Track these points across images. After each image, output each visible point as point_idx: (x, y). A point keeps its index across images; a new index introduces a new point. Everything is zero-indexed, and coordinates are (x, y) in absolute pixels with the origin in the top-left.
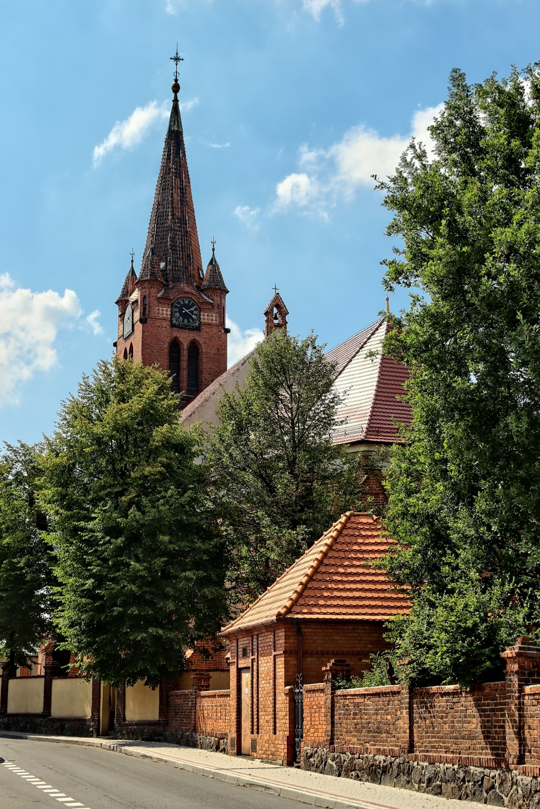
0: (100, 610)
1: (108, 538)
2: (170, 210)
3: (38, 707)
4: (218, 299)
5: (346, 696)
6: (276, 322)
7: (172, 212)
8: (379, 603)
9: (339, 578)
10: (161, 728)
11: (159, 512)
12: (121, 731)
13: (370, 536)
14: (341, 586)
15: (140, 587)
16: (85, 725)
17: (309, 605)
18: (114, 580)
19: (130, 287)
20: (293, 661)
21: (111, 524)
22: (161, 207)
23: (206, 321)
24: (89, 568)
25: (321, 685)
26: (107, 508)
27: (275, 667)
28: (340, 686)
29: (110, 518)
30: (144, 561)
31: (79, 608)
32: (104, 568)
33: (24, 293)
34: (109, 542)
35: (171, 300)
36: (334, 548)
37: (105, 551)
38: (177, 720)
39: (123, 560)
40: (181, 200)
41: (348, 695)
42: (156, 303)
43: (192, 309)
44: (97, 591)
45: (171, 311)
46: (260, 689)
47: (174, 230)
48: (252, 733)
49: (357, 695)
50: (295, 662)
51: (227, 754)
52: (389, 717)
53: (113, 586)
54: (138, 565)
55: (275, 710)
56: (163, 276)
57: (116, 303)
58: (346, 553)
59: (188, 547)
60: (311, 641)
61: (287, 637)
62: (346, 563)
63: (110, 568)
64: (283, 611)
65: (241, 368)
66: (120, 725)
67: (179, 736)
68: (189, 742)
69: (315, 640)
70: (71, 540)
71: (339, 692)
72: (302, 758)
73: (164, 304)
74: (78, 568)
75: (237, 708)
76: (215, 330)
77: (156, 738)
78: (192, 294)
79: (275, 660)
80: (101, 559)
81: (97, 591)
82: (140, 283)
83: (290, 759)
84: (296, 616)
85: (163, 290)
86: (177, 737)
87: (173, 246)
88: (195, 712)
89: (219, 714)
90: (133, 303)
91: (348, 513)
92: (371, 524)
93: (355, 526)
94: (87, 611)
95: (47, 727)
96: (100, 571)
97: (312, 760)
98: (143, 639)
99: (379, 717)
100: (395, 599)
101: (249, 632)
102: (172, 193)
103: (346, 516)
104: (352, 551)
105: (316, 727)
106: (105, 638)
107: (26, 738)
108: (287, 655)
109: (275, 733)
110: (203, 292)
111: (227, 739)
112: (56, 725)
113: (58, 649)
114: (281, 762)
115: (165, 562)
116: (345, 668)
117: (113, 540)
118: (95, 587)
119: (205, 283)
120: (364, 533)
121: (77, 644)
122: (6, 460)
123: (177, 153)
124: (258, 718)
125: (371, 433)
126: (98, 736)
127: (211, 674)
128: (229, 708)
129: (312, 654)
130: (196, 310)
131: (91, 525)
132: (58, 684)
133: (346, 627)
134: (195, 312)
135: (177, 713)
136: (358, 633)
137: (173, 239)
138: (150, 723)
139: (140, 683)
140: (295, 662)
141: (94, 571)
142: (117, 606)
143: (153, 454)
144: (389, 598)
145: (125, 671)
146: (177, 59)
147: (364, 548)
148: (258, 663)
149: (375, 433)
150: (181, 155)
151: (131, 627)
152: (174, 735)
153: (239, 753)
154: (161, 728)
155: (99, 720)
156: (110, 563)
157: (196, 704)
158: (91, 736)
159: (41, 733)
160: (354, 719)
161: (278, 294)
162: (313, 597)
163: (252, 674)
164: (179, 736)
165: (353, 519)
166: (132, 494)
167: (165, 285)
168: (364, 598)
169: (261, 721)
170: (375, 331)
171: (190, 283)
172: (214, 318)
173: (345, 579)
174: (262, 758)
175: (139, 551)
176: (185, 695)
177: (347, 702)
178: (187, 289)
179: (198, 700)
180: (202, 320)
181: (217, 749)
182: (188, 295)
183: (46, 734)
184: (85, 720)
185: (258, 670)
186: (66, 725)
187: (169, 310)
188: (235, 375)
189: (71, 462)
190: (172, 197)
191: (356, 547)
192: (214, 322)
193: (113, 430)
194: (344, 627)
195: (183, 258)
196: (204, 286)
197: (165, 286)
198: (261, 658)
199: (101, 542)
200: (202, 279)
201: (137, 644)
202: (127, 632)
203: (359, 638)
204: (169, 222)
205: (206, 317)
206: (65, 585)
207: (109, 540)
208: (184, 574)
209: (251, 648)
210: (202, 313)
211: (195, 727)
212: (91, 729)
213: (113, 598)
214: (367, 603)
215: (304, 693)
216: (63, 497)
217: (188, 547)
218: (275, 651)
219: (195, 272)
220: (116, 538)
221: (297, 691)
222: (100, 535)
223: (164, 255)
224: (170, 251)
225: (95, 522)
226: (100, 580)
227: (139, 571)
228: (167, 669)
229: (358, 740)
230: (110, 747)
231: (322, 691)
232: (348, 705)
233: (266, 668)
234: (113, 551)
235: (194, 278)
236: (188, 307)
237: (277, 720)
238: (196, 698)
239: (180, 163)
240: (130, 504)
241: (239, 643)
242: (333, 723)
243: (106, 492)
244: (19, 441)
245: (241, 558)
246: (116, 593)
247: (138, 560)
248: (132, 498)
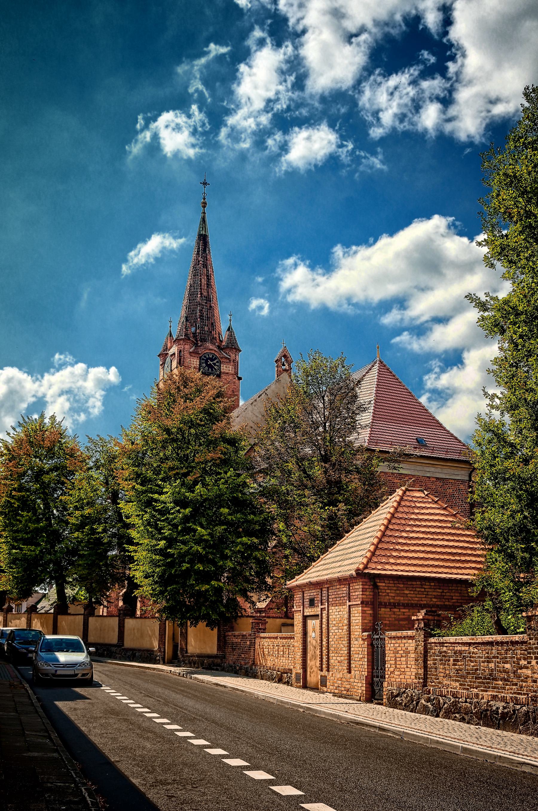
0: (170, 565)
3: (114, 639)
5: (443, 643)
6: (284, 367)
8: (441, 564)
10: (219, 661)
12: (184, 661)
14: (406, 548)
15: (204, 549)
18: (184, 543)
25: (410, 633)
27: (349, 616)
30: (207, 528)
33: (80, 367)
34: (178, 511)
36: (396, 516)
37: (175, 518)
41: (446, 643)
42: (189, 356)
43: (215, 362)
45: (200, 362)
46: (330, 634)
50: (371, 612)
51: (291, 685)
52: (507, 666)
54: (203, 530)
56: (194, 337)
62: (408, 529)
66: (183, 656)
67: (238, 668)
68: (250, 672)
70: (146, 509)
71: (432, 640)
75: (303, 649)
80: (172, 525)
83: (368, 696)
84: (372, 572)
87: (201, 316)
90: (171, 355)
93: (411, 499)
94: (159, 566)
96: (170, 534)
97: (398, 699)
98: (207, 591)
99: (492, 665)
100: (453, 560)
101: (318, 585)
103: (402, 490)
104: (411, 519)
105: (403, 670)
106: (175, 588)
107: (106, 662)
109: (350, 672)
111: (291, 674)
115: (225, 529)
116: (436, 618)
117: (182, 510)
118: (166, 548)
119: (224, 344)
122: (88, 450)
123: (204, 250)
126: (164, 663)
127: (267, 620)
129: (385, 606)
130: (217, 362)
131: (163, 498)
132: (129, 623)
133: (414, 583)
135: (234, 650)
137: (201, 311)
138: (209, 656)
139: (202, 625)
140: (371, 612)
142: (185, 562)
148: (328, 611)
152: (231, 666)
153: (305, 686)
155: (164, 652)
156: (180, 528)
158: (159, 664)
159: (115, 659)
163: (321, 621)
164: (238, 668)
165: (408, 493)
166: (197, 474)
167: (195, 344)
169: (332, 661)
174: (334, 693)
175: (203, 520)
176: (243, 636)
178: (211, 347)
179: (258, 641)
183: (120, 659)
184: (153, 651)
185: (328, 617)
191: (413, 516)
194: (413, 583)
197: (196, 345)
200: (221, 341)
203: (425, 593)
206: (141, 544)
208: (240, 539)
209: (319, 599)
213: (182, 556)
214: (431, 563)
216: (138, 475)
218: (349, 601)
219: (217, 336)
220: (185, 509)
221: (376, 637)
226: (171, 542)
227: (203, 535)
229: (461, 685)
230: (179, 674)
231: (411, 638)
233: (338, 616)
236: (212, 360)
241: (305, 595)
242: (425, 667)
243: (174, 472)
244: (98, 436)
245: (280, 531)
247: (202, 527)
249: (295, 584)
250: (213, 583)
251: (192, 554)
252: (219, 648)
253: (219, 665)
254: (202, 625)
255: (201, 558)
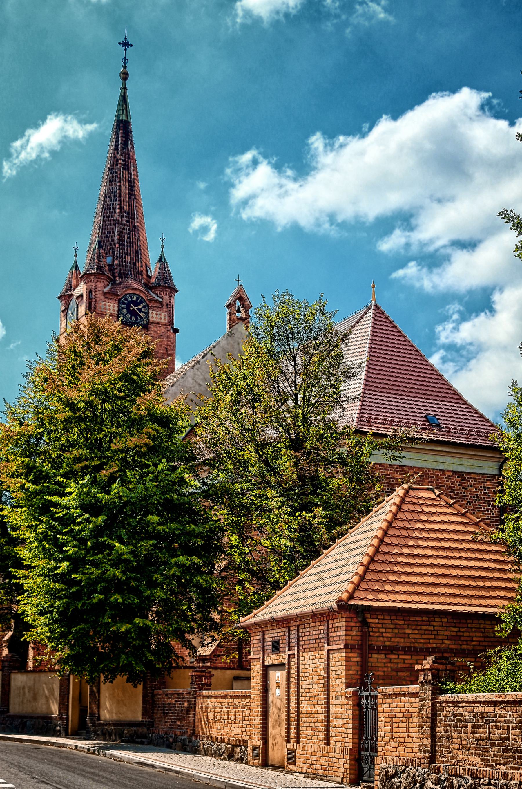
0: (76, 597)
1: (87, 516)
2: (117, 203)
4: (168, 297)
5: (458, 702)
7: (120, 205)
9: (406, 561)
10: (145, 730)
11: (147, 489)
12: (95, 732)
13: (434, 513)
14: (408, 570)
15: (124, 573)
16: (51, 723)
17: (373, 591)
18: (96, 564)
19: (74, 282)
20: (355, 658)
21: (87, 500)
22: (108, 199)
23: (154, 319)
24: (64, 548)
26: (84, 482)
28: (448, 690)
29: (88, 494)
30: (129, 544)
31: (54, 595)
32: (81, 550)
34: (88, 520)
35: (118, 295)
36: (394, 525)
38: (167, 722)
39: (105, 541)
40: (129, 194)
41: (463, 702)
42: (102, 298)
44: (73, 576)
45: (119, 307)
47: (122, 224)
48: (288, 741)
49: (480, 702)
51: (247, 763)
53: (93, 570)
54: (123, 547)
55: (328, 717)
56: (110, 270)
57: (59, 298)
58: (409, 531)
59: (179, 529)
60: (377, 634)
61: (348, 629)
63: (88, 551)
64: (345, 596)
65: (202, 360)
66: (94, 725)
67: (171, 740)
68: (188, 746)
69: (382, 633)
70: (42, 518)
71: (443, 698)
72: (377, 778)
73: (111, 299)
74: (50, 549)
76: (163, 329)
77: (139, 740)
78: (141, 291)
79: (328, 656)
80: (78, 540)
81: (73, 576)
82: (86, 276)
84: (360, 603)
85: (110, 285)
86: (168, 739)
87: (121, 241)
88: (194, 714)
89: (233, 718)
90: (78, 298)
91: (406, 486)
92: (433, 499)
93: (415, 501)
94: (60, 598)
95: (5, 724)
96: (76, 552)
97: (395, 780)
98: (128, 631)
100: (474, 587)
102: (120, 186)
103: (403, 488)
104: (416, 529)
105: (402, 740)
106: (83, 629)
108: (349, 650)
109: (328, 744)
110: (151, 290)
111: (246, 746)
112: (17, 722)
113: (25, 639)
114: (339, 779)
115: (153, 545)
117: (93, 519)
119: (153, 280)
120: (426, 509)
121: (48, 634)
123: (125, 144)
124: (298, 725)
125: (362, 423)
126: (67, 736)
127: (213, 672)
128: (248, 711)
129: (378, 650)
130: (144, 307)
131: (65, 501)
134: (143, 310)
135: (165, 714)
136: (434, 626)
137: (120, 233)
138: (131, 724)
139: (121, 679)
141: (70, 552)
143: (136, 424)
144: (467, 586)
145: (105, 666)
146: (126, 44)
147: (429, 526)
149: (367, 423)
150: (130, 146)
151: (113, 617)
152: (162, 738)
153: (265, 764)
154: (145, 730)
155: (67, 719)
157: (195, 704)
160: (473, 732)
161: (241, 285)
162: (377, 581)
163: (289, 672)
164: (171, 740)
165: (411, 493)
167: (111, 280)
168: (437, 584)
169: (303, 729)
170: (360, 320)
171: (138, 280)
172: (163, 317)
173: (412, 561)
174: (306, 773)
176: (179, 694)
177: (460, 710)
178: (135, 286)
179: (199, 701)
180: (150, 319)
181: (231, 756)
182: (136, 292)
184: (51, 718)
186: (28, 723)
187: (116, 305)
188: (195, 368)
189: (39, 431)
190: (120, 189)
191: (419, 525)
192: (163, 321)
193: (90, 395)
194: (417, 619)
195: (130, 254)
196: (153, 283)
197: (113, 282)
198: (302, 654)
199: (79, 520)
200: (150, 277)
201: (117, 637)
202: (109, 623)
203: (435, 632)
204: (116, 215)
205: (154, 315)
206: (34, 567)
207: (88, 518)
208: (175, 559)
210: (150, 312)
211: (194, 730)
212: (58, 728)
213: (92, 584)
214: (443, 590)
215: (379, 696)
216: (29, 469)
217: (179, 529)
218: (328, 645)
220: (97, 516)
221: (364, 694)
222: (76, 512)
223: (110, 249)
224: (117, 245)
225: (70, 498)
226: (77, 563)
227: (123, 554)
228: (155, 665)
229: (483, 760)
230: (89, 749)
231: (414, 695)
232: (461, 715)
233: (313, 666)
234: (91, 531)
235: (142, 275)
236: (136, 304)
237: (331, 729)
238: (195, 698)
239: (129, 154)
240: (112, 479)
241: (266, 636)
242: (433, 736)
246: (96, 578)
247: (121, 542)
248: (114, 473)
249: (252, 621)
250: (137, 621)
251: (106, 581)
252: (145, 712)
253: (145, 736)
254: (121, 679)
255: (118, 586)
